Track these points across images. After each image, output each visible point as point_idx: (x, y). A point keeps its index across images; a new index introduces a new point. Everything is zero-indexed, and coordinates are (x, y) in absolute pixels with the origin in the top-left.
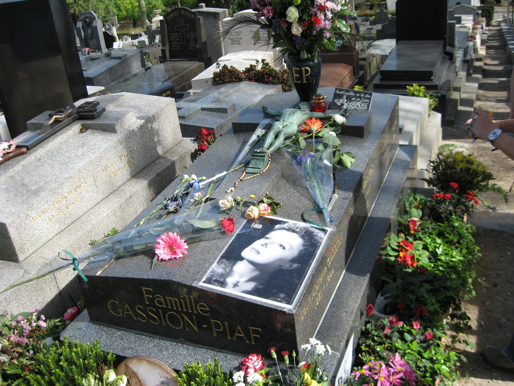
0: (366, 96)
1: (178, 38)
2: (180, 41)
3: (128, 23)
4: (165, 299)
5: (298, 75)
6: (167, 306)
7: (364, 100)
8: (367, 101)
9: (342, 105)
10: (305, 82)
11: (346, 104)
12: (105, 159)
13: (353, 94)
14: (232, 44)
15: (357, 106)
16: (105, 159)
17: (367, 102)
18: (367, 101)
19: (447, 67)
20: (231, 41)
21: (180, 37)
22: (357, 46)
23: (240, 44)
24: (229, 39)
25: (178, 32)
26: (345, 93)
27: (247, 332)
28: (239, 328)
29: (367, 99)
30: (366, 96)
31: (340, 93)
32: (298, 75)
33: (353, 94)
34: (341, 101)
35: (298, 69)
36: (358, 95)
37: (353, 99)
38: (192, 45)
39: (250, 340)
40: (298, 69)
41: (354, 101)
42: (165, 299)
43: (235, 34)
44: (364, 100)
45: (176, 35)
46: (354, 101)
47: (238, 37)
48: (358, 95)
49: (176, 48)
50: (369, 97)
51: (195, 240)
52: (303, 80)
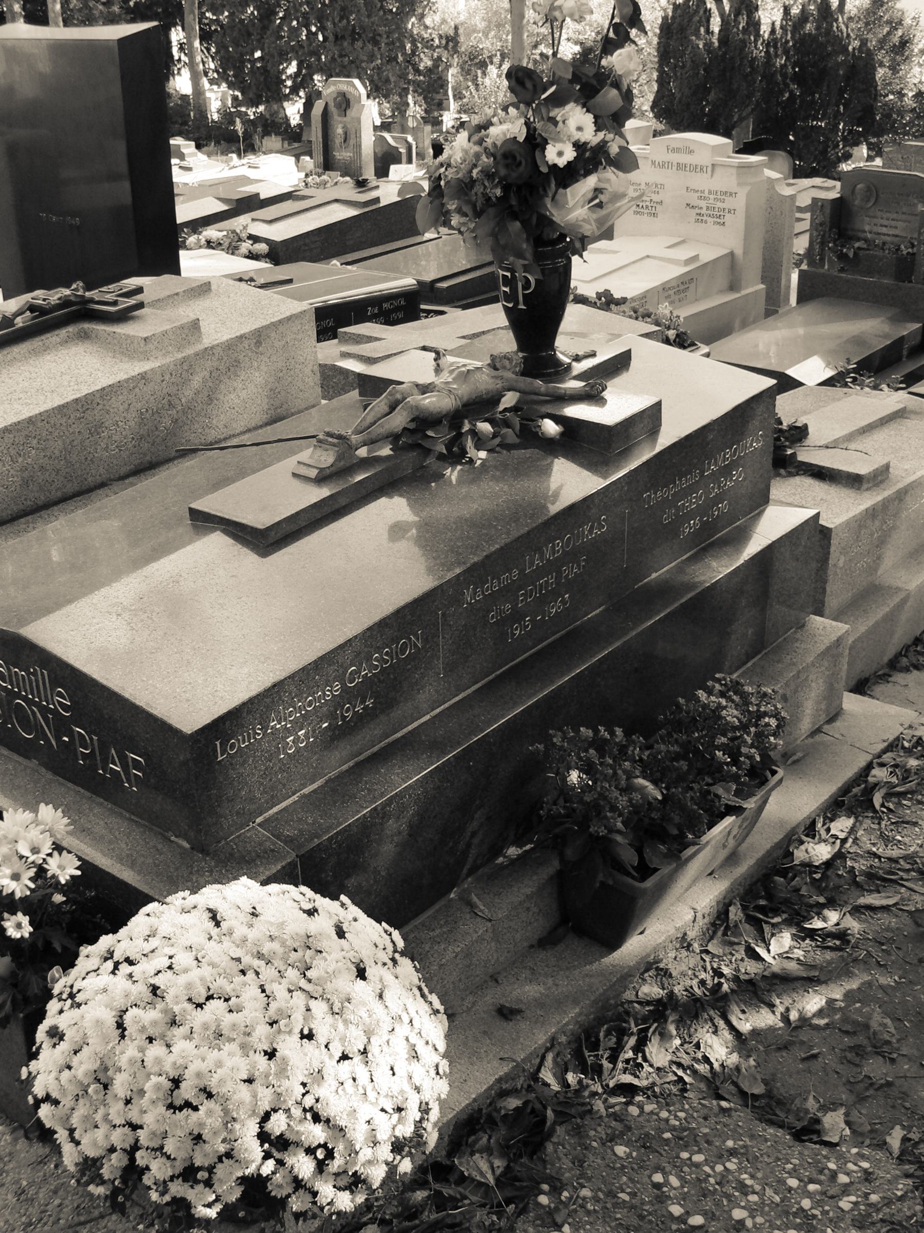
4: (9, 670)
5: (507, 289)
6: (41, 700)
10: (522, 307)
12: (100, 407)
27: (125, 767)
28: (113, 751)
32: (507, 289)
35: (508, 274)
39: (129, 781)
40: (508, 274)
47: (656, 198)
52: (517, 303)
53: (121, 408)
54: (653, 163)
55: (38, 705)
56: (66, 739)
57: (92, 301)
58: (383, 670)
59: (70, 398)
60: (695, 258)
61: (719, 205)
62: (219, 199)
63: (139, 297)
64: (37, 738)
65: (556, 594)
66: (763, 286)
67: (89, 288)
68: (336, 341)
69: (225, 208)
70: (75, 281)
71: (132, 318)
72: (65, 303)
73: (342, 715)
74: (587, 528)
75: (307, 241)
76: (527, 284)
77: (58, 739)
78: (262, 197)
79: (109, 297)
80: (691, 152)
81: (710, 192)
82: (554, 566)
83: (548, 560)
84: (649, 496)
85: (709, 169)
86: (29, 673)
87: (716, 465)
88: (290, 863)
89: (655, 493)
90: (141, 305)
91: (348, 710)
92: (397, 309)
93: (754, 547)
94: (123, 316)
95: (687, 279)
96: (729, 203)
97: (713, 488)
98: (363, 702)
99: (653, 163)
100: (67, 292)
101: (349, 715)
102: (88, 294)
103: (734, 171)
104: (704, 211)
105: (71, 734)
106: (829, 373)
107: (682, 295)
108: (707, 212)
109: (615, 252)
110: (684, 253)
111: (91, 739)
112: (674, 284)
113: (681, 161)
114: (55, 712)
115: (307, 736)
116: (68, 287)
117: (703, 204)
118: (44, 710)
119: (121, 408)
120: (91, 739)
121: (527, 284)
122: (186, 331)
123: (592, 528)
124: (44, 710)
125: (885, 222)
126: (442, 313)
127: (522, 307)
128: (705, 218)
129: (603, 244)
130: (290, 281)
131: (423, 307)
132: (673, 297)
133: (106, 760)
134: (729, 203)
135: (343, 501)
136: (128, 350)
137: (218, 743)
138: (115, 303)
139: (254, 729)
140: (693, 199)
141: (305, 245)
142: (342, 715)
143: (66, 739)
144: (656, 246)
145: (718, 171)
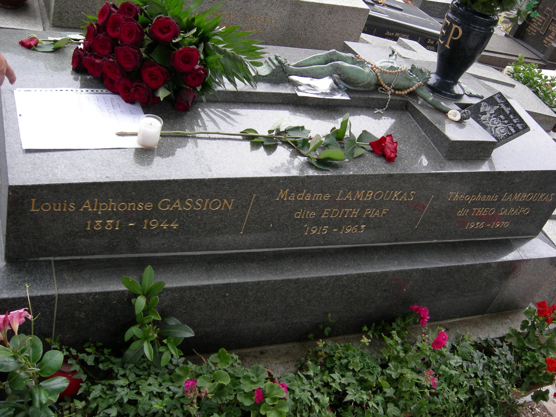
0: (518, 125)
1: (541, 22)
2: (540, 27)
7: (510, 127)
9: (485, 113)
10: (447, 46)
11: (488, 115)
13: (508, 112)
15: (497, 127)
17: (510, 131)
21: (542, 23)
25: (546, 16)
26: (502, 105)
30: (518, 125)
34: (488, 109)
36: (512, 117)
37: (502, 117)
38: (549, 40)
40: (449, 23)
41: (500, 119)
44: (510, 127)
45: (541, 18)
46: (500, 119)
48: (512, 117)
49: (531, 31)
50: (520, 128)
51: (228, 120)
58: (192, 211)
65: (354, 222)
68: (396, 42)
73: (148, 224)
74: (543, 195)
76: (456, 33)
82: (364, 206)
83: (358, 200)
91: (154, 223)
93: (511, 257)
97: (503, 211)
98: (169, 222)
101: (155, 226)
119: (236, 8)
121: (456, 33)
123: (401, 194)
126: (513, 86)
127: (447, 46)
130: (401, 10)
135: (256, 99)
137: (33, 200)
141: (434, 7)
142: (148, 224)
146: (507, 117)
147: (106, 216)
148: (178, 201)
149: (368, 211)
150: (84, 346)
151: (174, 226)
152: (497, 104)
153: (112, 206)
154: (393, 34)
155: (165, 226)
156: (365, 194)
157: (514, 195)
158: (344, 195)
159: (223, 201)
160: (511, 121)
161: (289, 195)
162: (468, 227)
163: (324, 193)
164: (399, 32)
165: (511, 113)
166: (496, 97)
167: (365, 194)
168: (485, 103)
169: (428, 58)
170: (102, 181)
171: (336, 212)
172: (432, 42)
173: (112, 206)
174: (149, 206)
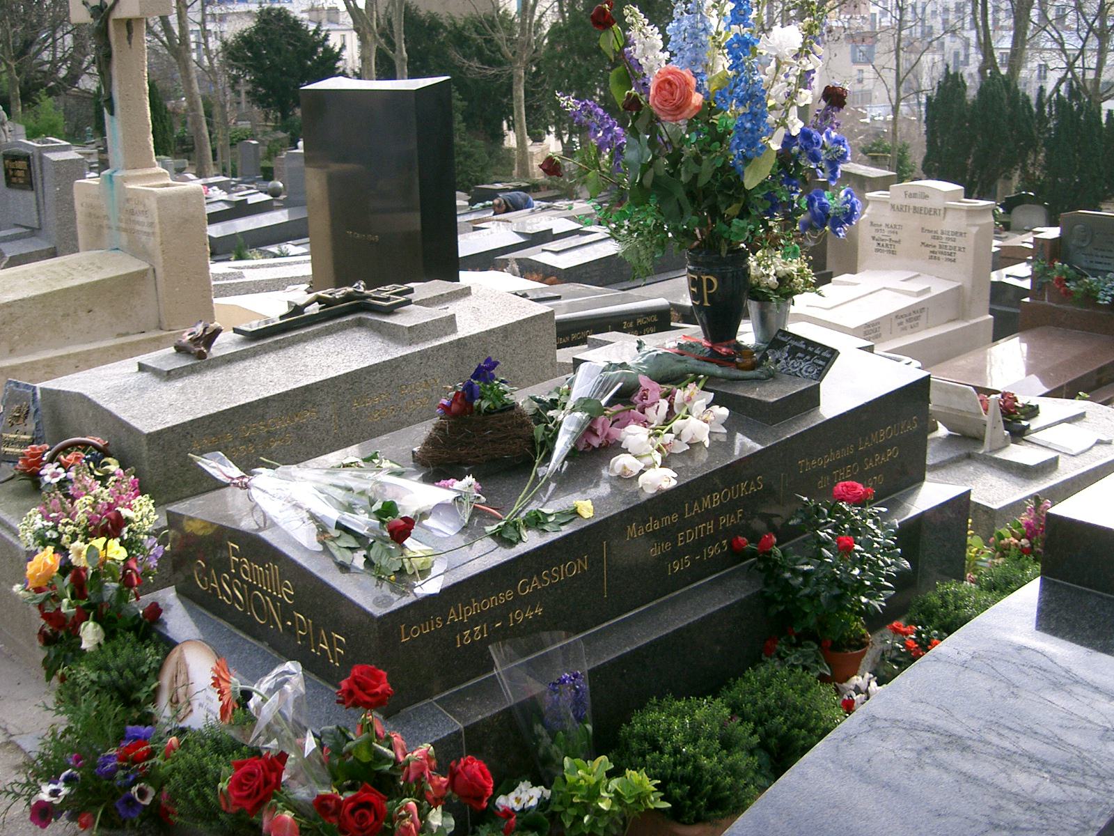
3: (625, 163)
4: (250, 566)
8: (821, 362)
10: (707, 304)
12: (366, 381)
13: (804, 346)
14: (877, 250)
16: (366, 381)
17: (820, 365)
18: (821, 362)
19: (952, 455)
20: (875, 242)
22: (770, 116)
23: (893, 253)
24: (873, 238)
29: (824, 359)
31: (783, 339)
33: (804, 346)
34: (778, 354)
36: (810, 349)
37: (799, 355)
39: (333, 658)
41: (800, 358)
42: (250, 566)
43: (886, 229)
44: (817, 361)
46: (800, 358)
47: (894, 237)
48: (810, 349)
50: (828, 356)
52: (702, 302)
53: (385, 384)
54: (893, 206)
55: (270, 595)
56: (289, 623)
57: (369, 297)
59: (342, 372)
60: (927, 290)
61: (951, 243)
62: (517, 233)
63: (409, 296)
64: (268, 624)
66: (991, 317)
67: (367, 288)
69: (522, 240)
70: (356, 281)
71: (397, 313)
72: (348, 297)
74: (743, 485)
75: (588, 269)
77: (283, 623)
78: (555, 232)
79: (384, 295)
80: (926, 197)
81: (942, 233)
84: (804, 463)
85: (942, 212)
86: (264, 569)
87: (870, 441)
88: (455, 733)
89: (810, 461)
90: (409, 302)
92: (650, 325)
94: (390, 311)
95: (918, 308)
96: (960, 242)
99: (893, 206)
100: (350, 289)
102: (367, 292)
103: (964, 214)
104: (937, 249)
105: (293, 619)
106: (1046, 390)
107: (915, 322)
108: (938, 251)
109: (856, 284)
110: (916, 286)
111: (307, 622)
112: (906, 312)
113: (917, 205)
114: (282, 600)
115: (481, 631)
116: (351, 286)
117: (936, 243)
118: (274, 599)
120: (307, 622)
122: (444, 324)
123: (748, 485)
124: (274, 599)
125: (1100, 260)
127: (707, 304)
128: (938, 255)
129: (846, 277)
130: (558, 298)
131: (672, 324)
132: (905, 324)
133: (318, 640)
134: (960, 242)
136: (394, 334)
138: (388, 299)
139: (434, 619)
140: (927, 238)
141: (586, 273)
143: (289, 623)
144: (893, 279)
145: (950, 214)
146: (806, 352)
147: (474, 621)
148: (535, 578)
149: (723, 520)
150: (892, 593)
151: (539, 611)
152: (784, 344)
153: (475, 608)
154: (568, 339)
155: (529, 615)
156: (711, 499)
157: (870, 438)
158: (691, 509)
159: (577, 563)
160: (812, 354)
161: (637, 530)
162: (672, 571)
163: (670, 514)
164: (584, 329)
165: (807, 347)
166: (779, 337)
167: (711, 499)
168: (771, 350)
169: (693, 332)
170: (460, 579)
171: (690, 533)
172: (631, 325)
173: (475, 608)
174: (509, 594)
